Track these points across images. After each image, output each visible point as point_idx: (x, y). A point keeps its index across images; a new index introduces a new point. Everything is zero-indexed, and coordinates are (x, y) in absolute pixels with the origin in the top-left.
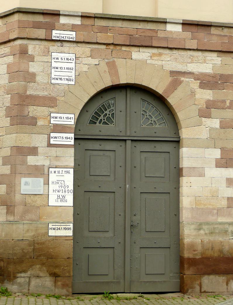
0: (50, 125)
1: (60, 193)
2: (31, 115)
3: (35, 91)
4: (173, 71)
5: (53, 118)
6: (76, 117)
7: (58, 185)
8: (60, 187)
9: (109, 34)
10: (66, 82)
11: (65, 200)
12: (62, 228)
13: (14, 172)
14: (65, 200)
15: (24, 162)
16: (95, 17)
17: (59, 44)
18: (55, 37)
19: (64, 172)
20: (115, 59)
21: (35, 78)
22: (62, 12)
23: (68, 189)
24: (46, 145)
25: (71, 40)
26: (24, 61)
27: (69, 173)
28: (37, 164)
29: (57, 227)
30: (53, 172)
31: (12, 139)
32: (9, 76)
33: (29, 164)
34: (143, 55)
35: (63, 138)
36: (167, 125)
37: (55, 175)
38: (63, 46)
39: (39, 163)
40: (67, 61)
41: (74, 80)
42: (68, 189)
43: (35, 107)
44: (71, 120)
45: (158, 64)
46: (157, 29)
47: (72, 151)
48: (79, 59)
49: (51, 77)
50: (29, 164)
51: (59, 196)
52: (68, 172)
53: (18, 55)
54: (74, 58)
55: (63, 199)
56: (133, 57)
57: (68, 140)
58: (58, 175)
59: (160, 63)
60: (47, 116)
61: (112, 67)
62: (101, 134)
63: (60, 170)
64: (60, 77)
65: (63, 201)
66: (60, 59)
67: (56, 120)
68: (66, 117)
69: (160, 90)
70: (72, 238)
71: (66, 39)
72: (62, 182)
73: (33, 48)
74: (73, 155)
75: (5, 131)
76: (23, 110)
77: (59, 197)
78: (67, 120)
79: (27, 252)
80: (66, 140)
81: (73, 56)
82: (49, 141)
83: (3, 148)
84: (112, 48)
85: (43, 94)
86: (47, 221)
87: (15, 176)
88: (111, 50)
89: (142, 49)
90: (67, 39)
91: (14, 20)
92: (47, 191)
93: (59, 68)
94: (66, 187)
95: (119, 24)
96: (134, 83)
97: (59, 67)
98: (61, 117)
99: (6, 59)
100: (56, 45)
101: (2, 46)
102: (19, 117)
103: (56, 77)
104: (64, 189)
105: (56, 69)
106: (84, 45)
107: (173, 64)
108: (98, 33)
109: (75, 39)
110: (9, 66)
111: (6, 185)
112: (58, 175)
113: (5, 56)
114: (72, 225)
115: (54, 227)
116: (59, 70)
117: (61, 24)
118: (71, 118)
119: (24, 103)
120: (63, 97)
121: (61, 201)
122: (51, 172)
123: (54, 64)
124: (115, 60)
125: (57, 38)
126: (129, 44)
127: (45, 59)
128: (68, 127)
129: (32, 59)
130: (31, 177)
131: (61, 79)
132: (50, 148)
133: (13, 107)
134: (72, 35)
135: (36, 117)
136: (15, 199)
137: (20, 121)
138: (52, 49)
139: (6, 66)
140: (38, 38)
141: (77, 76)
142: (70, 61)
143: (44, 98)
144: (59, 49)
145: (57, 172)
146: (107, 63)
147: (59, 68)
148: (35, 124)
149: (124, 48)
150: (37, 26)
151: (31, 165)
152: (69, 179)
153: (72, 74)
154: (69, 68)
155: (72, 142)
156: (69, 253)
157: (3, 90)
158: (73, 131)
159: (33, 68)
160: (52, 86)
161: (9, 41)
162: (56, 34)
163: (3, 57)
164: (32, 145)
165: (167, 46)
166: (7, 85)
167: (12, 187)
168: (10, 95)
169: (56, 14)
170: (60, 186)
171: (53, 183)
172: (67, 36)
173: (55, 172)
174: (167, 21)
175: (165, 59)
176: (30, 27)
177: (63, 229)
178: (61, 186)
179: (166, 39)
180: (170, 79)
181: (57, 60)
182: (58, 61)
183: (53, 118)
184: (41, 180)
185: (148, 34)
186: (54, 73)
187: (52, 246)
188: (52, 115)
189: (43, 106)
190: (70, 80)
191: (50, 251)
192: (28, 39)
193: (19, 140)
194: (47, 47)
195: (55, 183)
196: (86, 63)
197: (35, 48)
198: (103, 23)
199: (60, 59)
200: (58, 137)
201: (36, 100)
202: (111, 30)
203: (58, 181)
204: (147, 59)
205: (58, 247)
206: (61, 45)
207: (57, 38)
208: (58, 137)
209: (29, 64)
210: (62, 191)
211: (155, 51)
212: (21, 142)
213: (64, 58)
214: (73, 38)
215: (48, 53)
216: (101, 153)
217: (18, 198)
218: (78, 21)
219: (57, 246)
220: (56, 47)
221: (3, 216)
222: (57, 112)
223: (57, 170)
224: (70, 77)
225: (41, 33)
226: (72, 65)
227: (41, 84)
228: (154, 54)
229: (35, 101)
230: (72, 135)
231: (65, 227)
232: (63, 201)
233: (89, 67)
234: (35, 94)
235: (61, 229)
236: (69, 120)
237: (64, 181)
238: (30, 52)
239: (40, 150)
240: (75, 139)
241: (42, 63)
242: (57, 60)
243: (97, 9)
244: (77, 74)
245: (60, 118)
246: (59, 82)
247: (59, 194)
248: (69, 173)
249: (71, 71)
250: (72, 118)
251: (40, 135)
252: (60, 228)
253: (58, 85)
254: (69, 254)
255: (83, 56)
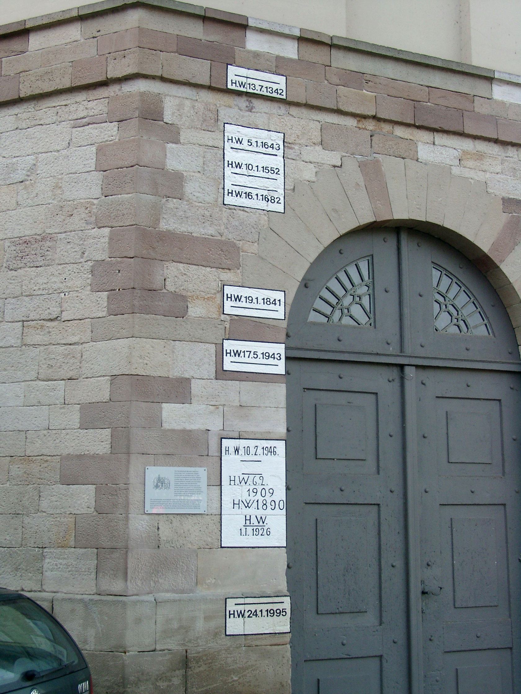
0: (223, 317)
1: (252, 511)
2: (170, 287)
3: (181, 223)
4: (509, 199)
5: (229, 299)
6: (290, 300)
7: (246, 488)
8: (252, 494)
9: (364, 91)
10: (263, 205)
11: (265, 528)
12: (261, 611)
13: (122, 446)
14: (265, 528)
15: (155, 421)
16: (332, 46)
17: (242, 102)
18: (234, 85)
19: (260, 451)
20: (380, 155)
21: (182, 186)
22: (254, 21)
23: (273, 498)
24: (213, 375)
25: (275, 95)
26: (153, 139)
27: (275, 453)
28: (189, 427)
29: (248, 608)
30: (232, 450)
31: (112, 356)
32: (106, 177)
33: (166, 426)
34: (442, 153)
35: (255, 356)
36: (493, 332)
37: (238, 458)
38: (252, 109)
39: (196, 425)
40: (264, 150)
41: (282, 201)
42: (273, 498)
43: (182, 265)
44: (277, 307)
45: (476, 178)
46: (472, 94)
47: (280, 391)
48: (293, 146)
49: (224, 189)
50: (166, 426)
51: (248, 518)
52: (272, 451)
53: (135, 122)
54: (281, 143)
55: (260, 528)
56: (419, 156)
57: (271, 361)
58: (247, 458)
59: (480, 176)
60: (213, 292)
61: (371, 171)
62: (343, 348)
63: (252, 443)
64: (248, 190)
65: (261, 532)
66: (245, 142)
67: (238, 304)
68: (264, 299)
69: (484, 243)
70: (288, 638)
71: (261, 93)
72: (257, 479)
73: (176, 104)
74: (283, 402)
75: (89, 331)
76: (143, 271)
77: (248, 522)
78: (266, 307)
79: (168, 686)
80: (265, 361)
81: (277, 139)
82: (220, 361)
83: (81, 379)
84: (371, 128)
85: (203, 231)
86: (221, 592)
87: (128, 461)
88: (368, 133)
89: (440, 139)
90: (265, 93)
91: (124, 28)
92: (217, 505)
93: (244, 167)
94: (267, 491)
95: (390, 70)
96: (427, 222)
97: (244, 163)
98: (250, 299)
99: (95, 132)
100: (237, 105)
101: (5, 119)
102: (139, 291)
103: (237, 189)
104: (261, 499)
105: (237, 167)
106: (305, 112)
107: (509, 180)
108: (340, 87)
109: (284, 93)
110: (101, 150)
111: (95, 486)
112: (247, 458)
113: (89, 124)
114: (287, 600)
115: (241, 608)
116: (244, 170)
117: (249, 52)
118: (277, 302)
119: (153, 255)
120: (256, 244)
121: (256, 532)
122: (227, 450)
123: (230, 156)
124: (380, 159)
125: (240, 87)
126: (412, 122)
127: (209, 138)
128: (269, 326)
129: (172, 134)
130: (172, 465)
131: (248, 195)
132: (224, 382)
133: (121, 262)
134: (277, 83)
135: (184, 293)
136: (128, 528)
137: (141, 303)
138: (224, 114)
139: (94, 149)
140: (191, 81)
141: (291, 191)
142: (270, 150)
143: (206, 241)
144: (243, 117)
145: (241, 451)
146: (362, 166)
147: (244, 167)
148: (182, 314)
149: (400, 131)
150: (188, 49)
151: (173, 430)
152: (273, 468)
153: (278, 185)
154: (269, 169)
155: (280, 368)
156: (281, 683)
157: (83, 216)
158: (283, 337)
159: (177, 159)
160: (226, 212)
161: (105, 84)
162: (236, 75)
163: (84, 126)
164: (175, 373)
165: (496, 137)
166: (95, 202)
167: (114, 495)
168: (107, 231)
169: (239, 25)
170: (251, 491)
171: (232, 483)
172: (265, 84)
173: (237, 450)
174: (496, 77)
175: (492, 169)
176: (171, 49)
177: (265, 613)
178: (255, 491)
179: (494, 120)
180: (505, 217)
181: (238, 146)
182: (241, 147)
183: (229, 299)
184: (202, 473)
185: (453, 102)
186: (231, 180)
187: (235, 666)
188: (228, 290)
189: (204, 263)
190: (273, 200)
191: (230, 681)
192: (163, 79)
193: (140, 357)
194: (212, 107)
195: (237, 481)
196: (312, 160)
197: (180, 106)
198: (353, 63)
199: (245, 142)
200: (244, 352)
201: (183, 248)
202: (370, 83)
203: (246, 477)
204: (451, 163)
205: (252, 665)
206: (247, 107)
207: (240, 87)
208: (244, 352)
209: (165, 148)
210: (255, 503)
211: (468, 145)
212: (145, 362)
213: (257, 142)
214: (280, 92)
215: (214, 123)
216: (342, 398)
217: (138, 525)
218: (290, 50)
219: (249, 663)
220: (234, 111)
221: (85, 577)
222: (240, 284)
223: (243, 443)
224: (272, 193)
225: (199, 70)
226: (277, 162)
227: (197, 204)
228: (465, 152)
229: (181, 250)
230: (280, 349)
231: (269, 607)
232: (261, 532)
233: (317, 169)
234: (183, 229)
235: (259, 613)
236: (272, 307)
237: (262, 477)
238: (168, 117)
239: (196, 387)
240: (287, 358)
241: (201, 149)
242: (238, 146)
243: (332, 27)
244: (289, 186)
245: (249, 299)
246: (243, 201)
247: (248, 511)
248: (275, 453)
249: (274, 176)
250: (280, 300)
251: (196, 343)
252: (256, 611)
253: (243, 210)
254: (283, 686)
255: (302, 141)
